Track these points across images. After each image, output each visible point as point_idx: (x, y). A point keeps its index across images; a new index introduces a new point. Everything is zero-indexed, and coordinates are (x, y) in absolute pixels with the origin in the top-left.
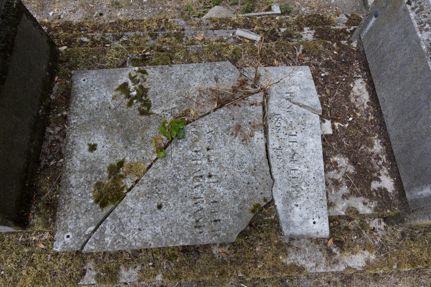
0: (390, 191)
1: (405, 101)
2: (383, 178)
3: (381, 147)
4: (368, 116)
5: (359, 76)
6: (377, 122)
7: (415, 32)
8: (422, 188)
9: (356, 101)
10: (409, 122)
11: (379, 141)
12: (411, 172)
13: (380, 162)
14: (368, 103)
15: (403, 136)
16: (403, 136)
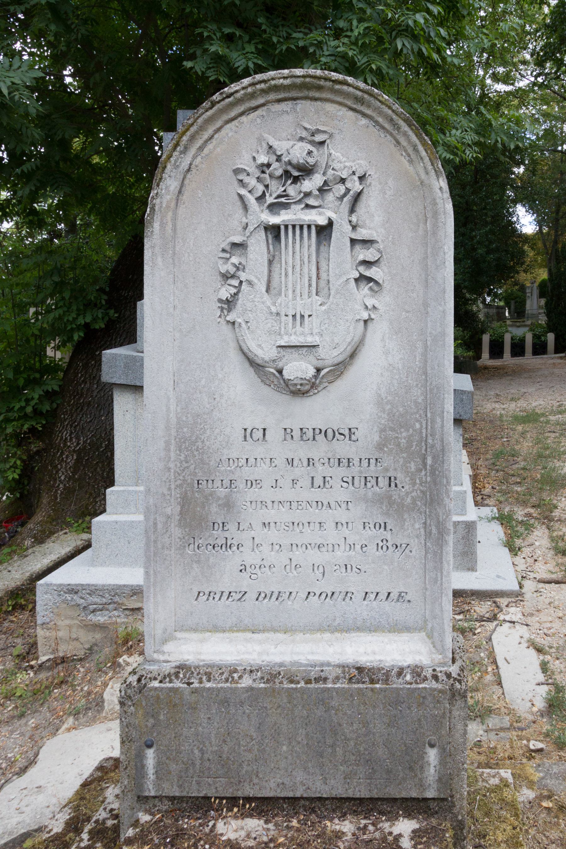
0: (417, 826)
1: (307, 744)
2: (396, 830)
3: (347, 822)
4: (288, 828)
5: (211, 824)
6: (304, 815)
7: (236, 688)
8: (427, 762)
9: (255, 838)
10: (338, 749)
11: (336, 821)
12: (401, 775)
13: (371, 828)
14: (266, 822)
15: (351, 768)
16: (351, 768)
